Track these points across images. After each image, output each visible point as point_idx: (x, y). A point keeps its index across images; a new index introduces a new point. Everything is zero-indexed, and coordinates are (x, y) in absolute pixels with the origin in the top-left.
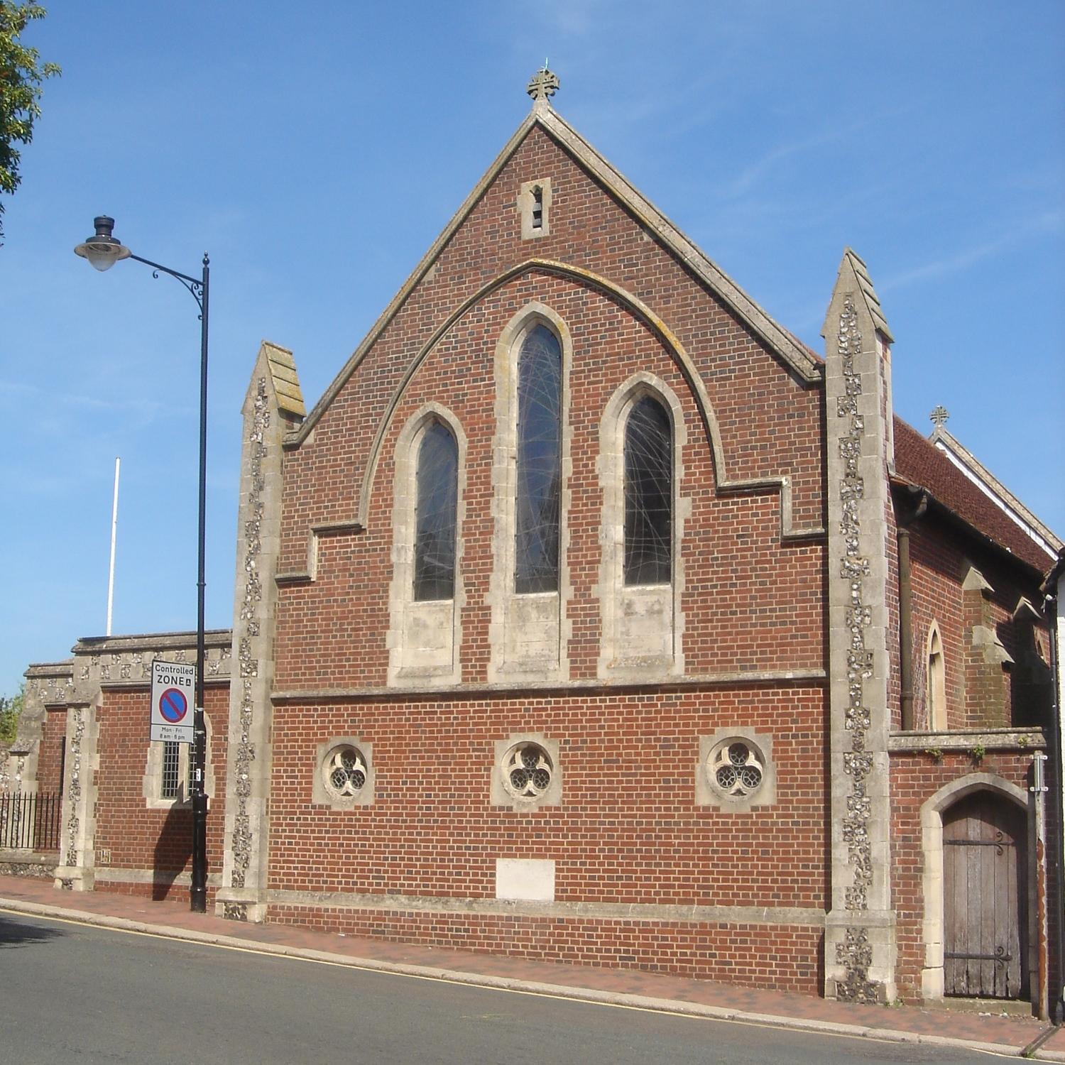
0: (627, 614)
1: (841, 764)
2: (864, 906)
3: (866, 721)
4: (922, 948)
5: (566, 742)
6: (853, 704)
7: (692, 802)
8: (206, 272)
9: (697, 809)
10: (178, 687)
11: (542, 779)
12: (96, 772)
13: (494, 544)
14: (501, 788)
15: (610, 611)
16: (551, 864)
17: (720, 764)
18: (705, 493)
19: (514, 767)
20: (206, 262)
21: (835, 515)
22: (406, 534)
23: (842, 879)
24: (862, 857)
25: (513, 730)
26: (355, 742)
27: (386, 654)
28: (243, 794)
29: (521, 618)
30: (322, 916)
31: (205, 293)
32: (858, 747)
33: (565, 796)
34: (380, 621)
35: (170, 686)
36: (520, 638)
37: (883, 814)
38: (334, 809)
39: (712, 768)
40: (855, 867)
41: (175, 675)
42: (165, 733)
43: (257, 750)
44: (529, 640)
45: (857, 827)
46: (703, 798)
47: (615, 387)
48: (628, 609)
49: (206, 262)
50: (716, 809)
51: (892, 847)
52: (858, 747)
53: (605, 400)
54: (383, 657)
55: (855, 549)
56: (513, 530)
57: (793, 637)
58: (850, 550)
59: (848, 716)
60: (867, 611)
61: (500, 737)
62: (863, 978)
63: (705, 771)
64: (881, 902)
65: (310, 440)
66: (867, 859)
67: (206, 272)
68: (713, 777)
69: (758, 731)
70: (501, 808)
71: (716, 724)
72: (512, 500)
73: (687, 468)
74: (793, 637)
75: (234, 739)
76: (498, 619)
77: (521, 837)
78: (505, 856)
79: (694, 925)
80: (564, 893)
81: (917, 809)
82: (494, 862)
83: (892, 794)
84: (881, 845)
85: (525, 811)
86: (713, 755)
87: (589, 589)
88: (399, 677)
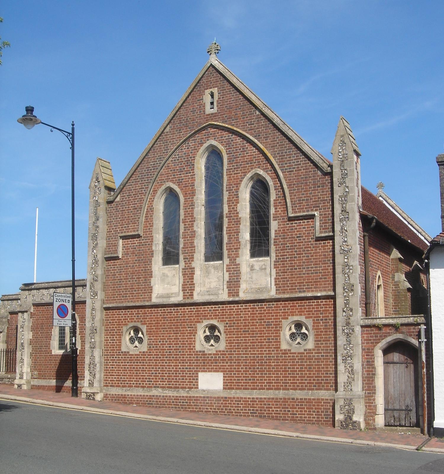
0: (251, 270)
1: (341, 331)
2: (351, 390)
3: (351, 313)
4: (375, 406)
5: (227, 324)
6: (346, 306)
7: (279, 348)
8: (73, 129)
9: (281, 350)
10: (64, 303)
11: (217, 339)
12: (31, 339)
13: (195, 241)
14: (200, 343)
15: (244, 269)
16: (221, 375)
17: (291, 332)
18: (283, 219)
19: (205, 334)
20: (73, 125)
21: (337, 228)
22: (159, 238)
23: (342, 378)
24: (350, 369)
25: (205, 319)
26: (139, 325)
27: (151, 288)
28: (93, 348)
29: (207, 272)
30: (126, 398)
31: (73, 138)
32: (348, 324)
33: (226, 346)
34: (149, 274)
35: (61, 303)
36: (207, 281)
37: (358, 352)
38: (131, 353)
39: (288, 333)
40: (347, 373)
41: (63, 298)
42: (59, 323)
43: (98, 329)
44: (211, 281)
45: (348, 357)
46: (284, 346)
47: (245, 175)
48: (252, 268)
49: (73, 125)
50: (290, 350)
51: (363, 365)
52: (348, 324)
53: (241, 181)
54: (149, 289)
55: (345, 242)
56: (203, 236)
57: (320, 279)
58: (343, 242)
59: (344, 311)
60: (351, 268)
61: (199, 322)
62: (351, 419)
63: (284, 335)
64: (358, 388)
65: (118, 199)
66: (352, 370)
67: (73, 129)
68: (288, 337)
69: (306, 318)
70: (200, 352)
71: (289, 315)
72: (203, 223)
73: (276, 209)
74: (320, 279)
75: (88, 325)
76: (198, 273)
77: (209, 363)
78: (202, 371)
79: (281, 399)
80: (227, 386)
81: (373, 349)
82: (197, 374)
83: (362, 343)
84: (358, 364)
85: (210, 352)
86: (288, 328)
87: (235, 260)
88: (157, 297)
